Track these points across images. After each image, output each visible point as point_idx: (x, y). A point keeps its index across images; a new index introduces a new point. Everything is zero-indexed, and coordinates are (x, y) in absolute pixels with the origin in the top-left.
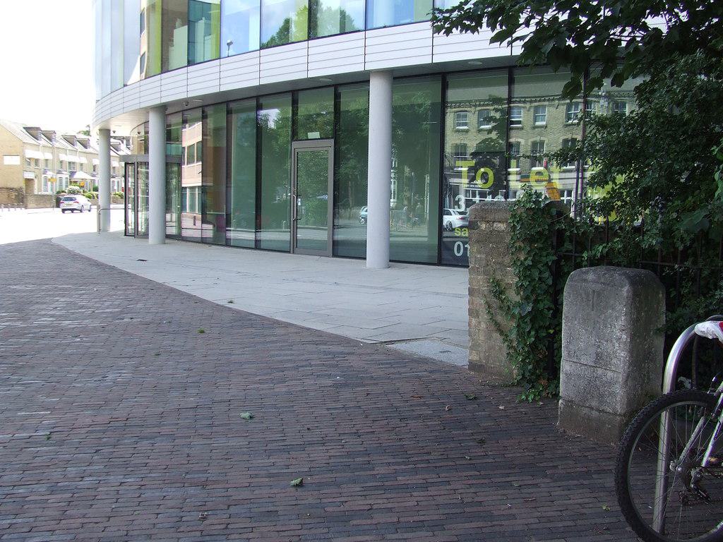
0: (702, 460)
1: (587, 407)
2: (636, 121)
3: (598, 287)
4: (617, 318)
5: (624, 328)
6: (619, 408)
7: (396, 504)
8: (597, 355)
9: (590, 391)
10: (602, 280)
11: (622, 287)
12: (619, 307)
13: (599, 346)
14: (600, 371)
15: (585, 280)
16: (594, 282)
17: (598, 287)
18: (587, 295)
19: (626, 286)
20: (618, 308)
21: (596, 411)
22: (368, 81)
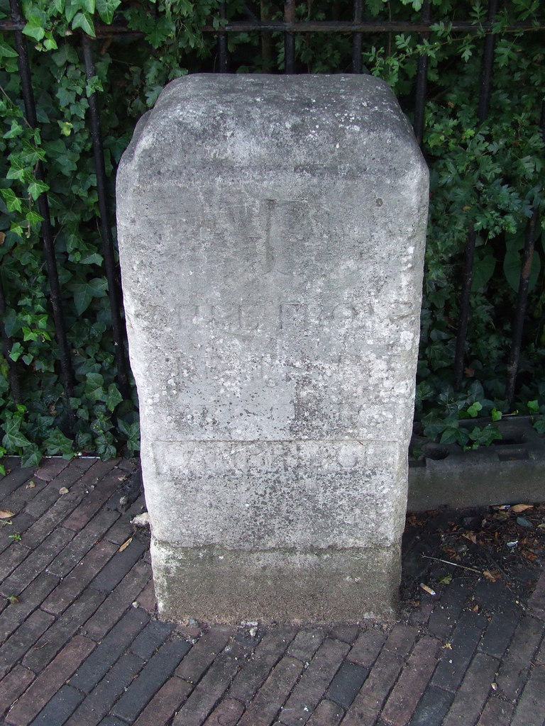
0: (430, 587)
1: (273, 549)
2: (482, 377)
3: (290, 185)
4: (378, 284)
5: (405, 311)
6: (392, 530)
7: (295, 655)
8: (299, 406)
9: (278, 510)
10: (300, 156)
11: (397, 173)
12: (384, 247)
13: (305, 381)
14: (309, 449)
15: (220, 166)
16: (262, 167)
17: (290, 185)
18: (243, 221)
19: (408, 167)
20: (381, 251)
21: (305, 552)
22: (73, 298)
